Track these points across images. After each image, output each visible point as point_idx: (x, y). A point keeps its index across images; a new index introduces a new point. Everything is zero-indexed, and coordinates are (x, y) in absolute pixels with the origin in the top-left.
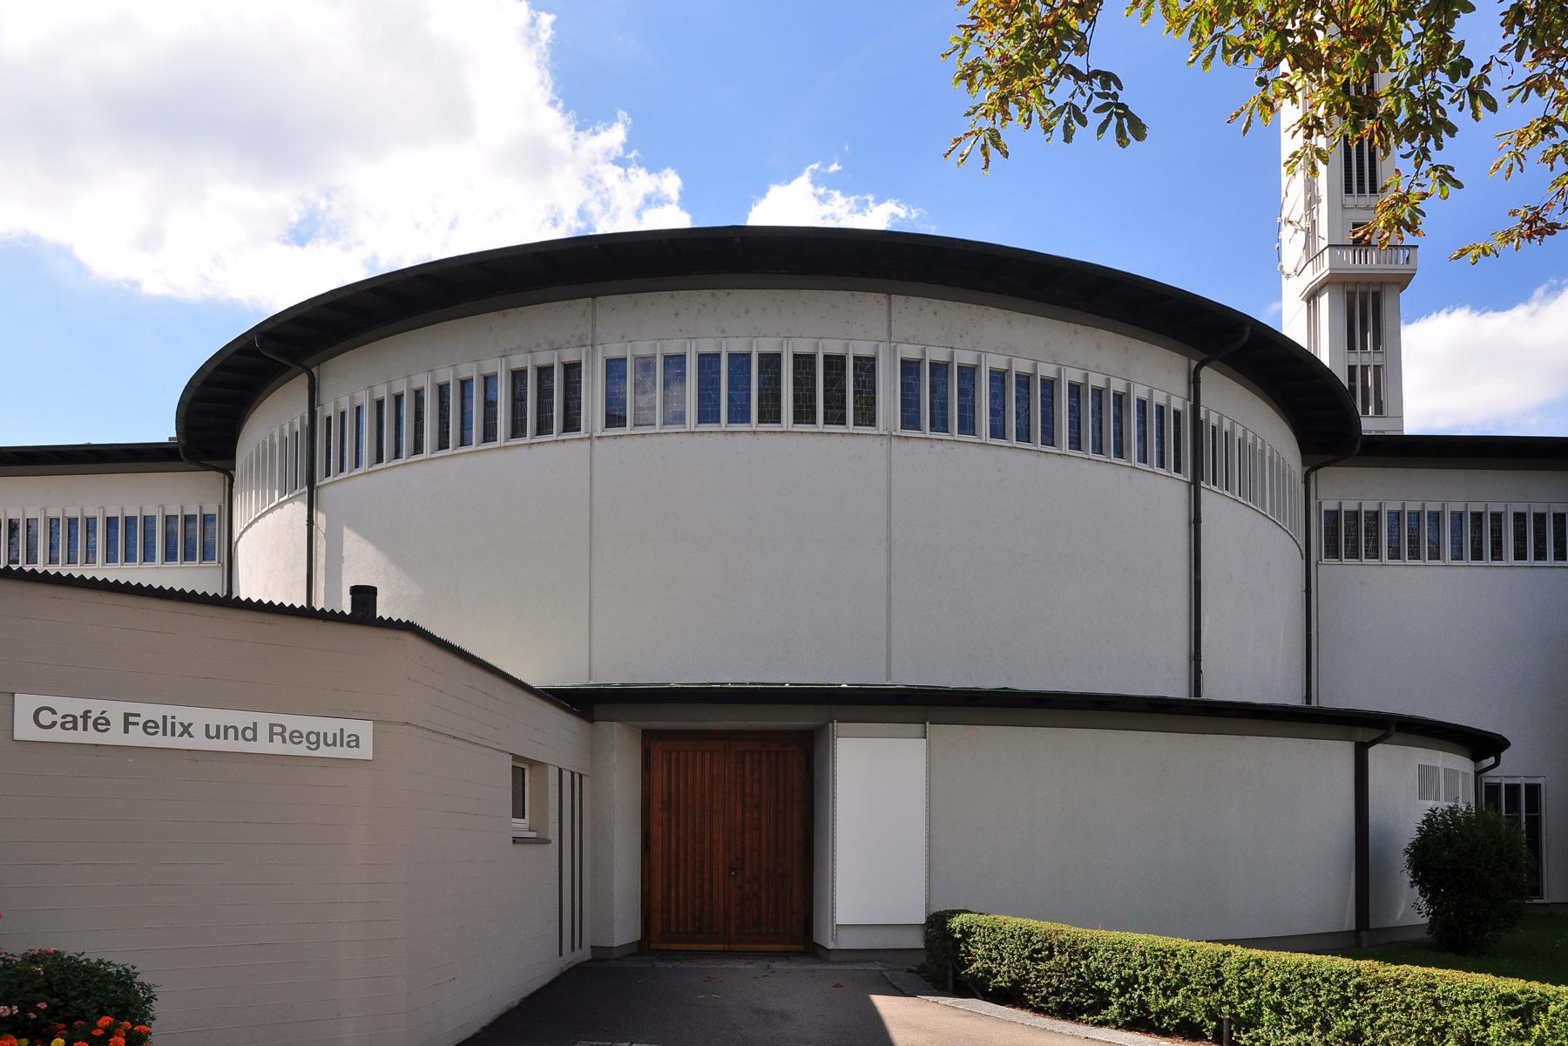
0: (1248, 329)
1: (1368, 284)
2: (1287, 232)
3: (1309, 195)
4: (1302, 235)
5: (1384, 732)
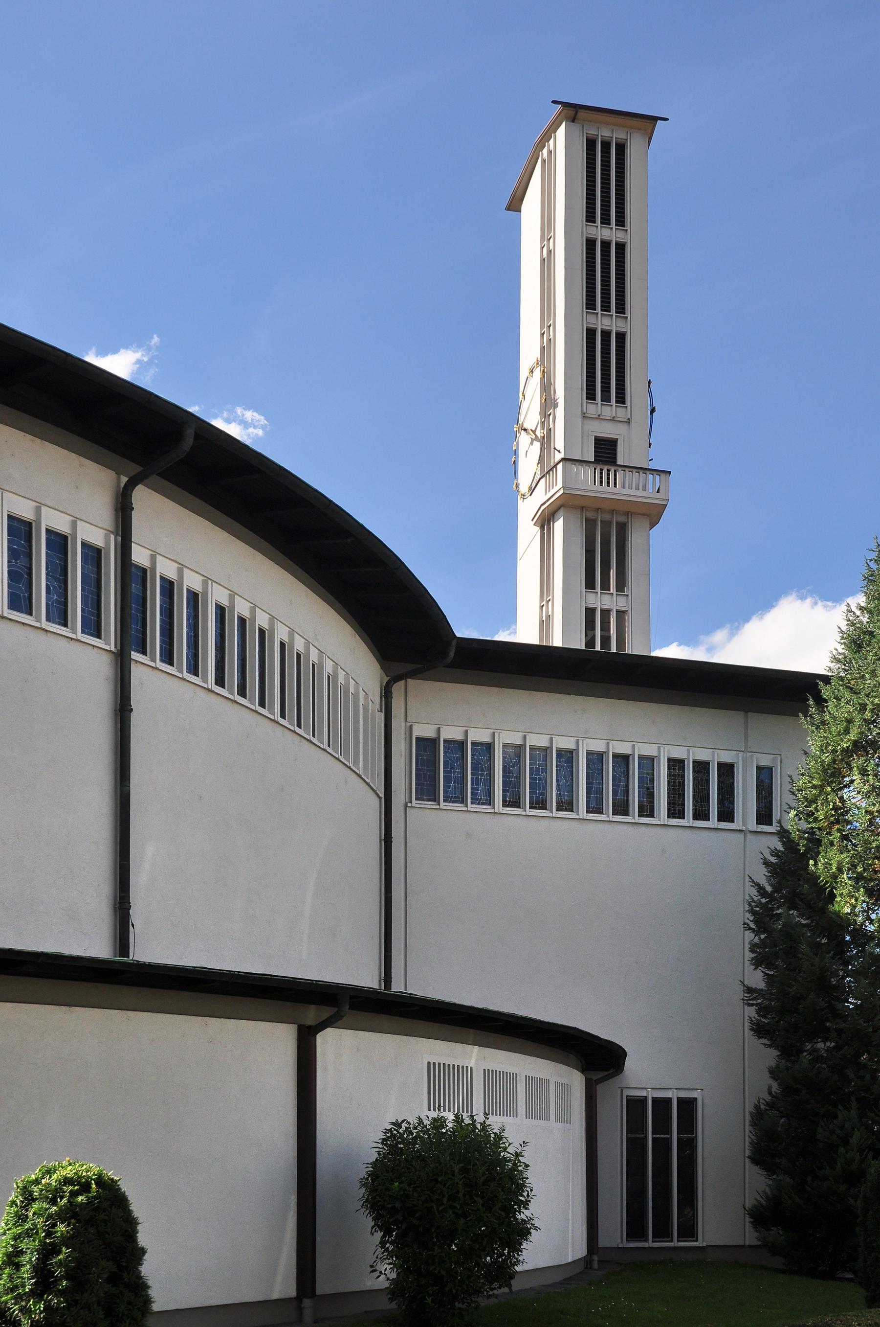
0: (190, 433)
1: (612, 512)
2: (524, 439)
3: (544, 398)
4: (537, 445)
5: (335, 1010)
